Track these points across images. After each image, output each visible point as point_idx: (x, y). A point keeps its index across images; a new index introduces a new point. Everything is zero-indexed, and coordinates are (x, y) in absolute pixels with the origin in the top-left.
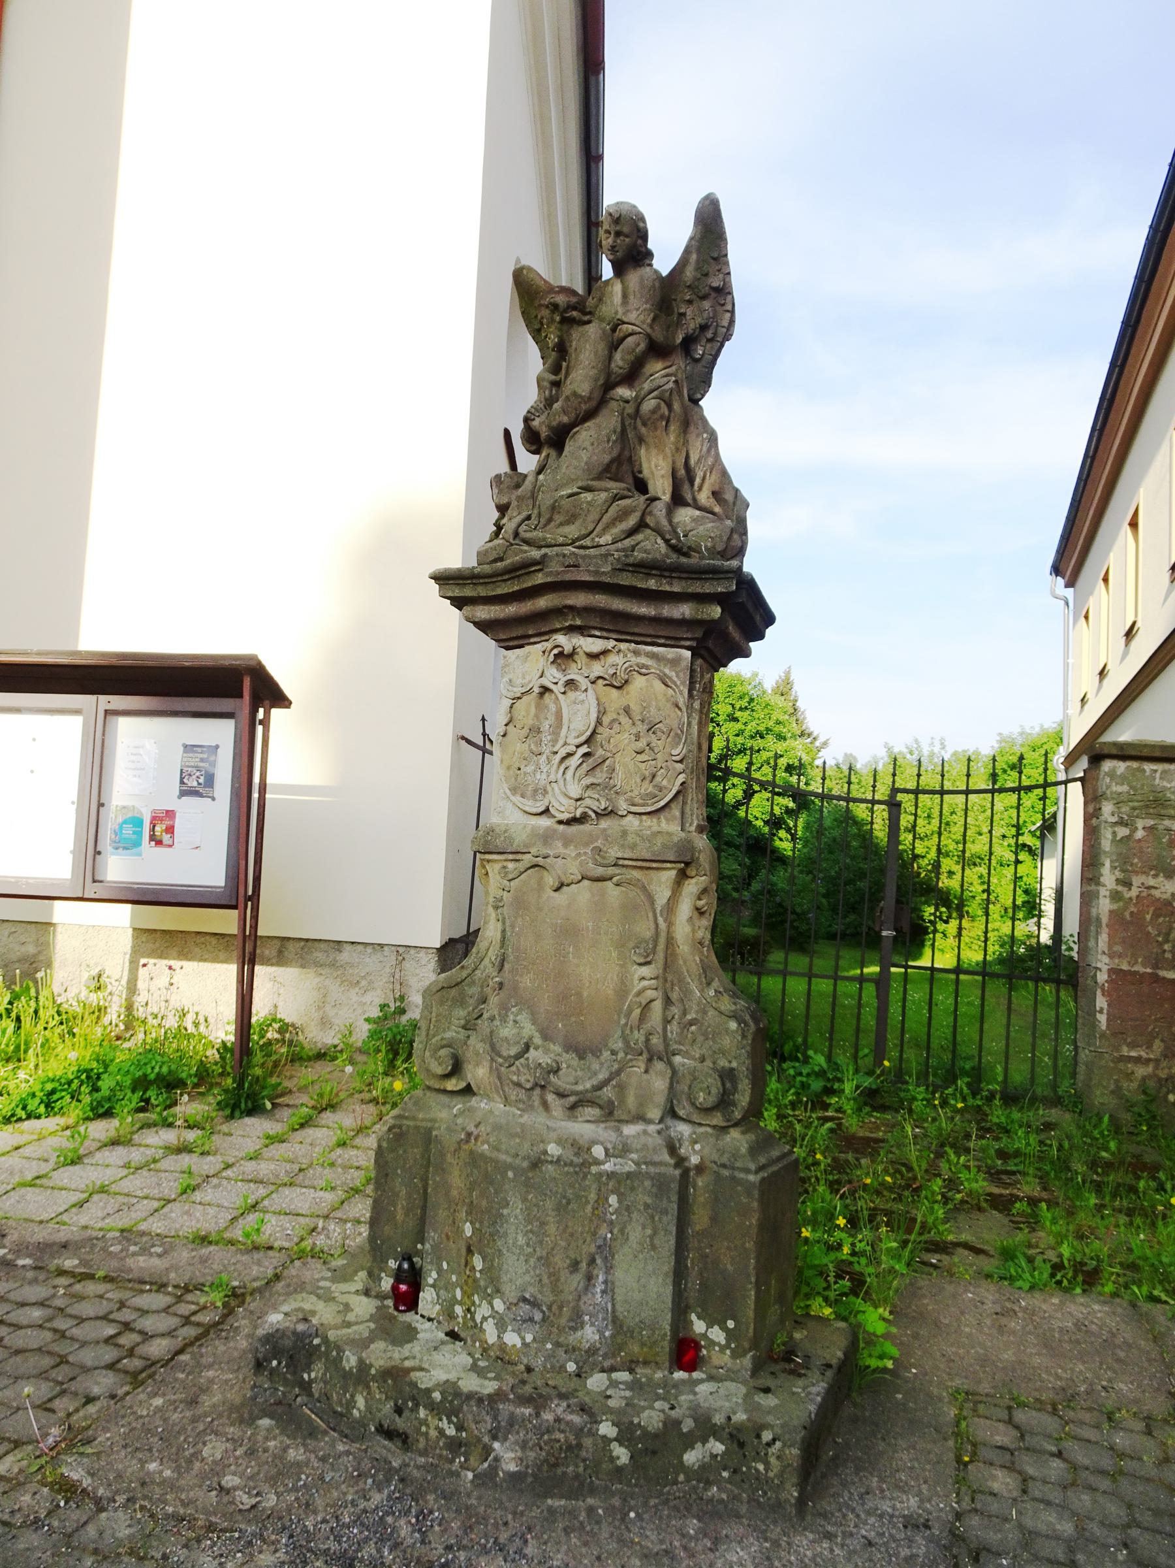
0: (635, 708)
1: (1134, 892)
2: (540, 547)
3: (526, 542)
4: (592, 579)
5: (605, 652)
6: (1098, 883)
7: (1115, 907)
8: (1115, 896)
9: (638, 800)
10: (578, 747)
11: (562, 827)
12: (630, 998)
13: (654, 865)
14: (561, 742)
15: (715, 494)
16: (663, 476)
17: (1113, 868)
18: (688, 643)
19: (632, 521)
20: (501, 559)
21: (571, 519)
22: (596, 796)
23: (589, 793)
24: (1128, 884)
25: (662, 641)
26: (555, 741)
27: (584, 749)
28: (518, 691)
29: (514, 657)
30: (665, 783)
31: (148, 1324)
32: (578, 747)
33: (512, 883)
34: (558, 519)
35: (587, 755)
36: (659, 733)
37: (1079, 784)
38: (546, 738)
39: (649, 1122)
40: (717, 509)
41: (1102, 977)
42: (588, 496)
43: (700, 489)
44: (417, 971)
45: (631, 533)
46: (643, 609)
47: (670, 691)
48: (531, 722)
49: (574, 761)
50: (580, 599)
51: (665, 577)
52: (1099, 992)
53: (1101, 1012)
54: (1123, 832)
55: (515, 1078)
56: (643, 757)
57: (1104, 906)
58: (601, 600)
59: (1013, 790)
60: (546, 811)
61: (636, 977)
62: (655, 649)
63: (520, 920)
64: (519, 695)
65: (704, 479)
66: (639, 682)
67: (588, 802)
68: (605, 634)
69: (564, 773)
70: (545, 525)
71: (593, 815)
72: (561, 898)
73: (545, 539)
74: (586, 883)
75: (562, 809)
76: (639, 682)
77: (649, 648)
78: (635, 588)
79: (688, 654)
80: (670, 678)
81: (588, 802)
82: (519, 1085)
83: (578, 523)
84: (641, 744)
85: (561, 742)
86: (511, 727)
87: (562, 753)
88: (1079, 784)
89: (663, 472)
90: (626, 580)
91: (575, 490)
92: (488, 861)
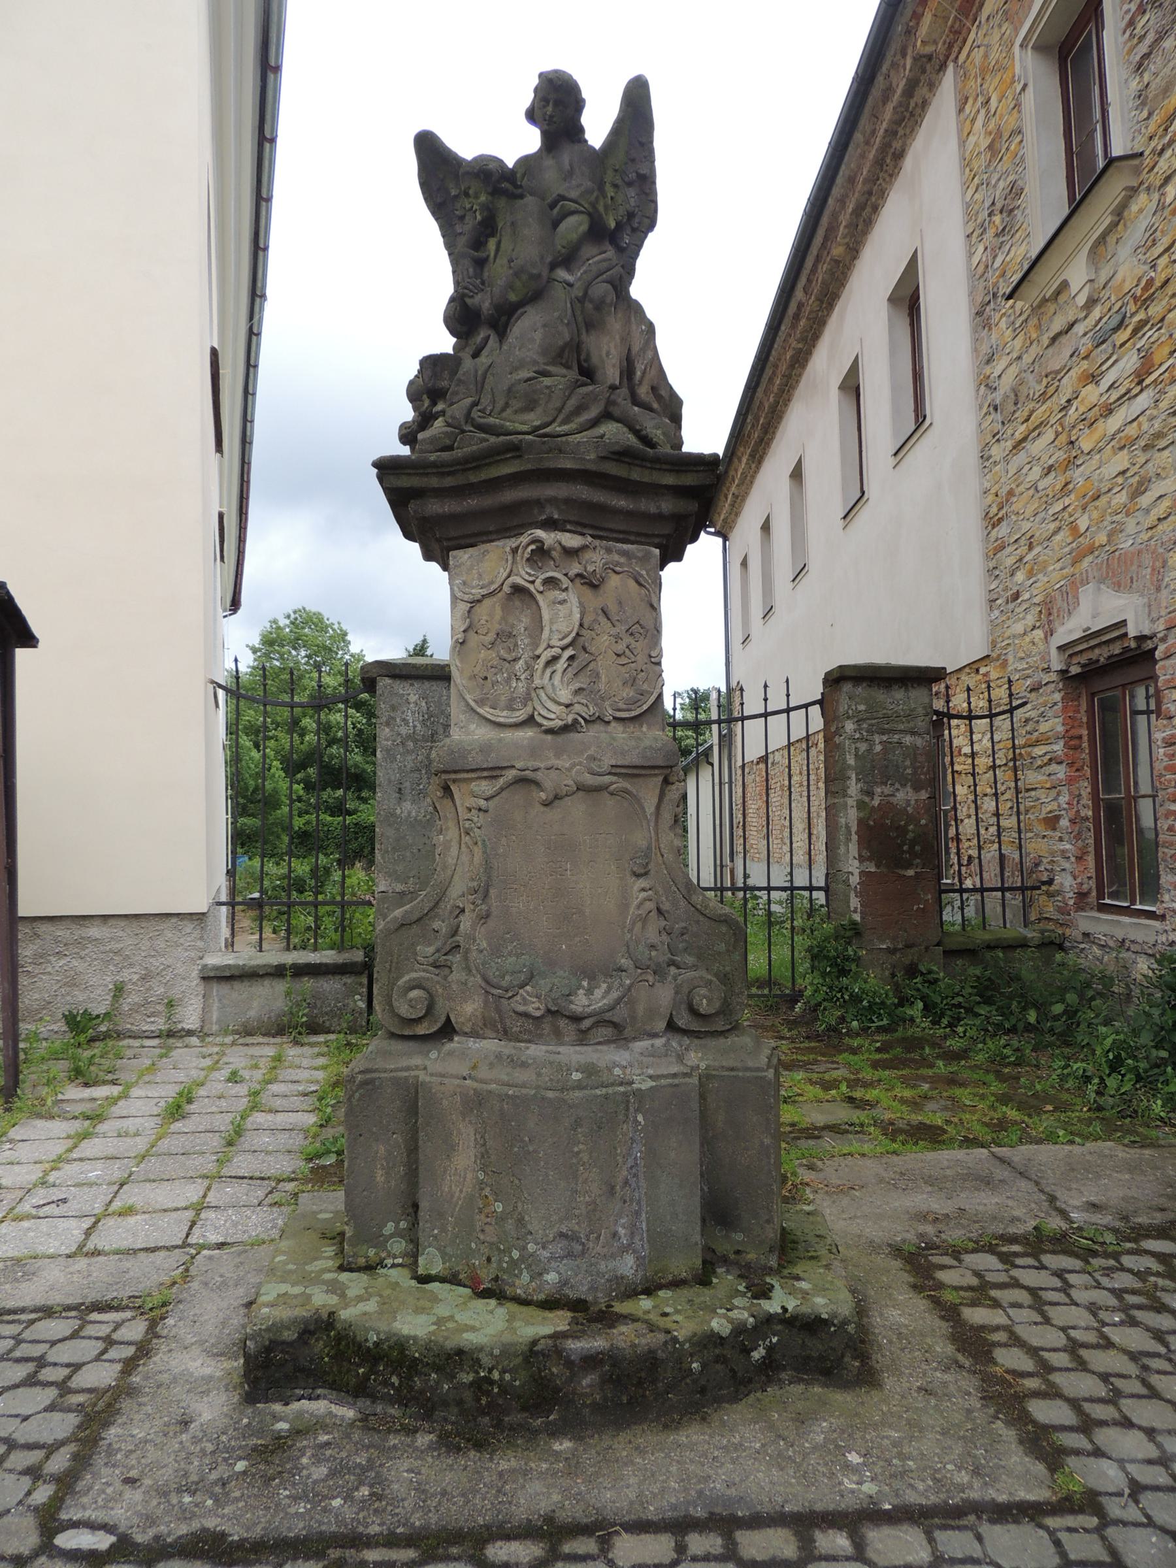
0: (613, 608)
1: (876, 803)
2: (498, 435)
3: (482, 428)
4: (578, 467)
5: (584, 548)
6: (845, 795)
7: (861, 815)
8: (861, 805)
9: (621, 705)
10: (563, 649)
11: (549, 737)
12: (631, 910)
13: (643, 772)
14: (543, 645)
15: (654, 389)
16: (614, 366)
17: (858, 780)
18: (657, 541)
19: (593, 412)
20: (449, 448)
21: (530, 406)
22: (585, 701)
23: (578, 698)
24: (870, 794)
25: (632, 538)
26: (536, 645)
27: (569, 652)
28: (477, 592)
29: (466, 556)
30: (645, 687)
31: (65, 1353)
32: (563, 649)
33: (490, 803)
34: (516, 404)
35: (572, 658)
36: (637, 635)
37: (818, 706)
38: (523, 641)
39: (655, 1035)
40: (655, 406)
41: (855, 880)
42: (547, 381)
43: (641, 382)
44: (182, 941)
45: (595, 423)
46: (622, 503)
47: (643, 591)
48: (497, 626)
49: (561, 665)
50: (561, 490)
51: (647, 468)
52: (852, 895)
53: (855, 911)
54: (863, 747)
55: (521, 1008)
56: (624, 660)
57: (851, 817)
58: (582, 492)
59: (760, 716)
60: (530, 721)
61: (635, 888)
62: (625, 547)
63: (504, 841)
64: (479, 597)
65: (644, 373)
66: (614, 581)
67: (577, 708)
68: (579, 529)
69: (551, 678)
70: (503, 410)
71: (582, 722)
72: (554, 814)
73: (502, 426)
74: (581, 794)
75: (553, 716)
76: (614, 581)
77: (619, 545)
78: (628, 481)
79: (657, 551)
80: (642, 576)
81: (577, 708)
82: (526, 1015)
83: (539, 410)
84: (621, 647)
85: (543, 645)
86: (471, 634)
87: (547, 655)
88: (818, 706)
89: (614, 361)
90: (612, 469)
91: (533, 374)
92: (454, 781)
